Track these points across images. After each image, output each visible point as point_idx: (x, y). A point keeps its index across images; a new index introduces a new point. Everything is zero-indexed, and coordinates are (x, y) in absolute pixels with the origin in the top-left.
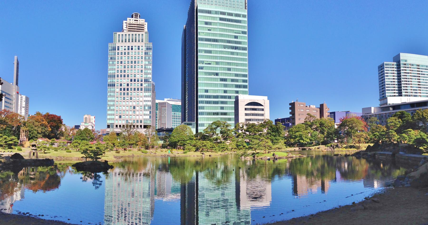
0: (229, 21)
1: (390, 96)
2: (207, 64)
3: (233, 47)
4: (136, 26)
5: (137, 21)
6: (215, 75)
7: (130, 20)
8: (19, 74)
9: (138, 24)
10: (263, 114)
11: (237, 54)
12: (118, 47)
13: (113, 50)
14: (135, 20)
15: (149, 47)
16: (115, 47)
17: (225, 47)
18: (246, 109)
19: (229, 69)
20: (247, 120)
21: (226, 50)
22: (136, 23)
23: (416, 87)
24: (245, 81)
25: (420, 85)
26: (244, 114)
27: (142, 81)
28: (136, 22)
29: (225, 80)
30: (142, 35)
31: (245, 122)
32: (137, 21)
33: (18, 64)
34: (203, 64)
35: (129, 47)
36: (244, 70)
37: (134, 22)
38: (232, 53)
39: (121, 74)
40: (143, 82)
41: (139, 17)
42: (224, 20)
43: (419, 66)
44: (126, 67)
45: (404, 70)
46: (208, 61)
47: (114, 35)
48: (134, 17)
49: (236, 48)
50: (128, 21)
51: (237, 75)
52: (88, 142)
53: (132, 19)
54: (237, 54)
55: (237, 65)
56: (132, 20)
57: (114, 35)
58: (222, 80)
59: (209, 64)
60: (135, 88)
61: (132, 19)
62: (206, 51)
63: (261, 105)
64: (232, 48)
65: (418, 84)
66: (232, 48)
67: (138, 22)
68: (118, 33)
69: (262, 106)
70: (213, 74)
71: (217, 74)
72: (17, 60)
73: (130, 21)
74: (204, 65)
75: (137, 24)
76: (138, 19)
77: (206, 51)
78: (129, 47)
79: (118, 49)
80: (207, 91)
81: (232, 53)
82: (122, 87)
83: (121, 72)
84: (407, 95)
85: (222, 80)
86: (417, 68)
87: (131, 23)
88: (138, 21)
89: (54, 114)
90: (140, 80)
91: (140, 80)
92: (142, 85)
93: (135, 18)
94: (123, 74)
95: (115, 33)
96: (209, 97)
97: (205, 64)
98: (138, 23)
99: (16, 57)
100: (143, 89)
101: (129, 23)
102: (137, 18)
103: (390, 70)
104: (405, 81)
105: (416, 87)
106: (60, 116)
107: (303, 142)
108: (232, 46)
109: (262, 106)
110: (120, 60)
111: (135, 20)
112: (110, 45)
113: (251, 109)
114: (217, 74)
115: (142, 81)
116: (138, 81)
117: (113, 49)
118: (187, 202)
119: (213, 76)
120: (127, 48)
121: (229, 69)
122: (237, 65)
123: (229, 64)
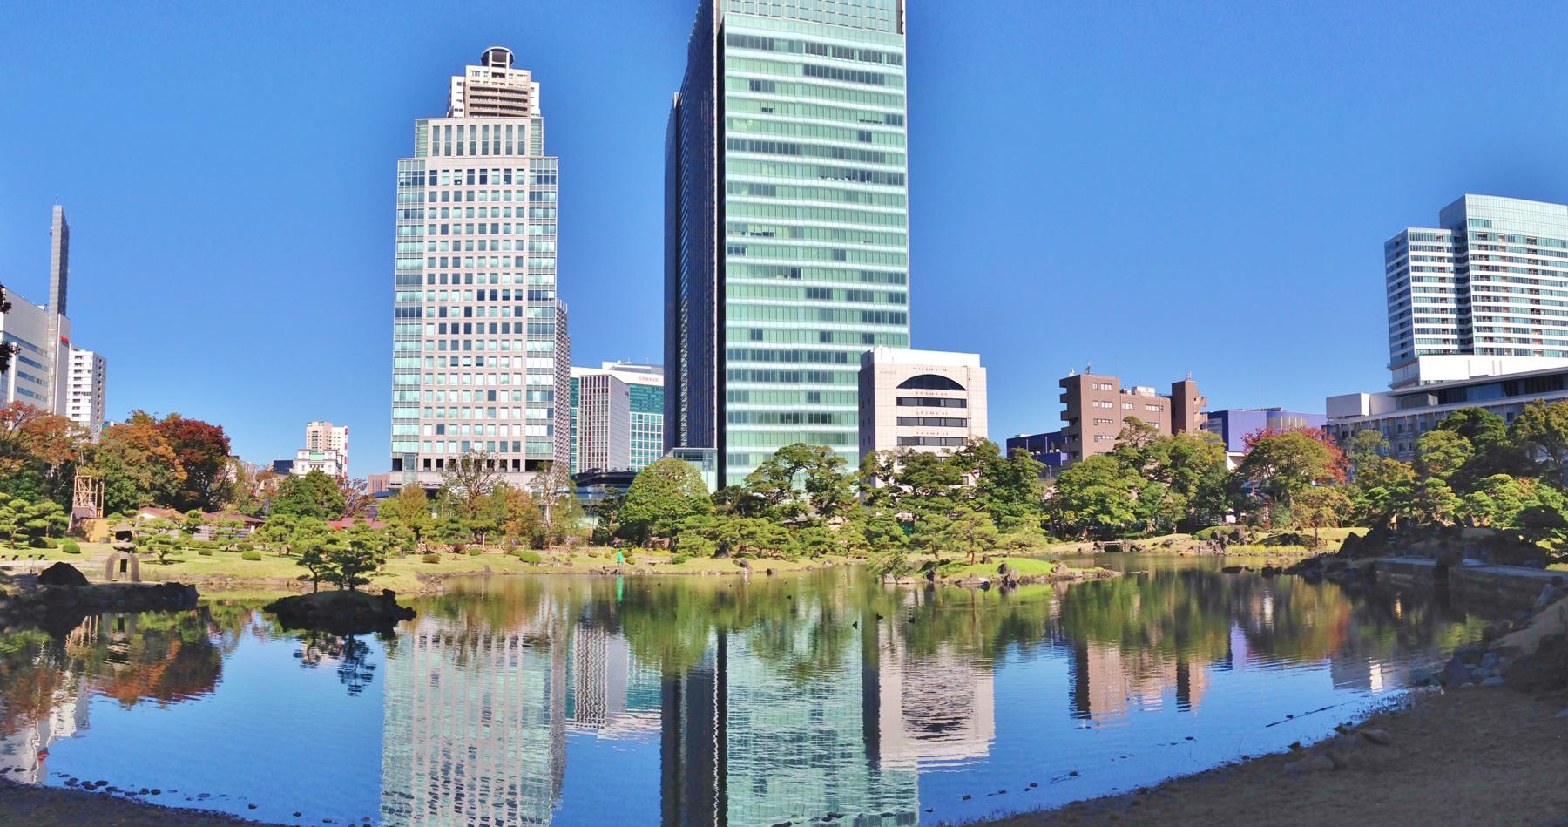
0: (840, 78)
1: (1430, 353)
2: (759, 234)
3: (855, 171)
4: (498, 94)
5: (502, 76)
6: (786, 277)
7: (477, 73)
8: (69, 271)
9: (506, 87)
10: (962, 419)
11: (870, 198)
12: (434, 172)
13: (415, 183)
14: (494, 75)
15: (546, 171)
16: (423, 173)
17: (824, 172)
18: (900, 401)
19: (840, 255)
20: (904, 441)
21: (830, 183)
22: (498, 86)
23: (1526, 321)
24: (896, 298)
25: (1538, 311)
26: (895, 419)
27: (519, 298)
28: (498, 79)
29: (824, 294)
30: (522, 127)
31: (899, 448)
32: (502, 76)
33: (65, 235)
34: (743, 233)
35: (471, 171)
36: (894, 258)
37: (491, 82)
38: (851, 196)
39: (444, 271)
40: (524, 303)
41: (508, 63)
42: (820, 75)
43: (1534, 241)
44: (463, 245)
45: (1481, 256)
46: (760, 225)
47: (419, 130)
48: (491, 62)
49: (865, 176)
50: (469, 78)
51: (867, 276)
52: (322, 522)
53: (485, 69)
54: (870, 198)
55: (868, 237)
56: (482, 74)
57: (419, 130)
58: (813, 293)
59: (766, 234)
60: (493, 322)
61: (482, 69)
62: (756, 189)
63: (955, 386)
64: (852, 175)
65: (1532, 310)
66: (849, 178)
67: (507, 81)
68: (433, 122)
69: (961, 388)
70: (780, 274)
71: (795, 273)
72: (64, 222)
73: (476, 78)
74: (747, 239)
75: (503, 87)
76: (507, 71)
77: (756, 189)
78: (471, 171)
79: (434, 181)
80: (757, 335)
81: (851, 196)
82: (449, 321)
83: (444, 265)
84: (1492, 350)
85: (813, 293)
86: (1529, 250)
87: (482, 85)
88: (507, 76)
89: (198, 419)
90: (512, 295)
91: (512, 295)
92: (518, 312)
93: (493, 65)
94: (450, 271)
95: (420, 123)
96: (766, 356)
97: (752, 234)
98: (506, 83)
99: (57, 210)
100: (525, 328)
101: (474, 85)
102: (503, 66)
103: (1429, 259)
104: (1483, 297)
105: (1526, 321)
106: (220, 427)
107: (1109, 521)
108: (848, 170)
109: (961, 388)
110: (439, 222)
111: (494, 75)
112: (402, 167)
113: (921, 401)
114: (795, 273)
115: (519, 298)
116: (506, 298)
117: (415, 179)
118: (687, 744)
119: (779, 281)
120: (464, 176)
121: (840, 255)
122: (868, 237)
123: (838, 234)
